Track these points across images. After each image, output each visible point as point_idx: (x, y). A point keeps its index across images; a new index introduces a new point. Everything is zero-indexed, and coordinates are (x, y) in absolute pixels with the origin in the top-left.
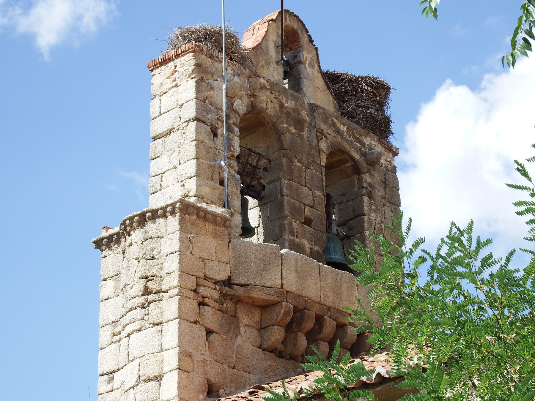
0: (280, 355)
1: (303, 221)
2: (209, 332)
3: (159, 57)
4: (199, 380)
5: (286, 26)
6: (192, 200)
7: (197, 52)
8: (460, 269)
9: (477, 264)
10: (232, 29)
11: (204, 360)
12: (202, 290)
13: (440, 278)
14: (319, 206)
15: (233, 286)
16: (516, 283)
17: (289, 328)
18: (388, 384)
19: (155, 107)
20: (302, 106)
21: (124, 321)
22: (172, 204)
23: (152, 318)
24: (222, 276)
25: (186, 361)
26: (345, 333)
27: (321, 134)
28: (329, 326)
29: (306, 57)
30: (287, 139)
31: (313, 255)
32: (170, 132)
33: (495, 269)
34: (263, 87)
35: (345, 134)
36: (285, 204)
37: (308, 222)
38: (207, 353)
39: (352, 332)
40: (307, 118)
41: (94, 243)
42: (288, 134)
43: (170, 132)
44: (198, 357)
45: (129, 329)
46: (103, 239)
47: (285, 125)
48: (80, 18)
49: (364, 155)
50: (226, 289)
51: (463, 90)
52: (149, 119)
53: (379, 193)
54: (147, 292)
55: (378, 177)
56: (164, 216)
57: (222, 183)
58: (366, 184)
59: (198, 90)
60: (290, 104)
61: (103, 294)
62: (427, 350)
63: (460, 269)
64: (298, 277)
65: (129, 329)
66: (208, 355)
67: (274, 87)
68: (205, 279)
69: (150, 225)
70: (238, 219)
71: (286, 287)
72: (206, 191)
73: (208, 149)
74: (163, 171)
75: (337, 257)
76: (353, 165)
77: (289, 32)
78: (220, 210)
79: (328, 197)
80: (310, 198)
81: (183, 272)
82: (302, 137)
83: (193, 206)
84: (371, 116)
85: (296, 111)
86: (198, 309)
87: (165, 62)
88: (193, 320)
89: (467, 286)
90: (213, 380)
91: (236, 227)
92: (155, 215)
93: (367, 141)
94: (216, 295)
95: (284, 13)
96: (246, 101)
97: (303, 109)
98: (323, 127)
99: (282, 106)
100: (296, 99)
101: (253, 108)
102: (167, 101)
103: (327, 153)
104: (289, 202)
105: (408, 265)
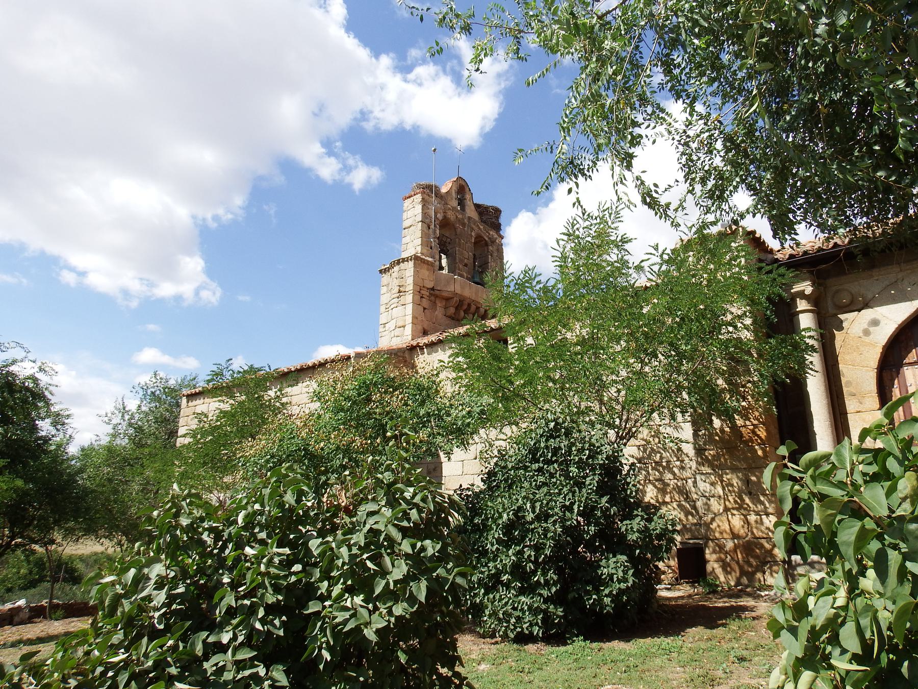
0: (453, 319)
2: (425, 309)
3: (407, 195)
4: (420, 327)
6: (419, 255)
7: (423, 193)
8: (527, 285)
9: (534, 283)
10: (437, 184)
12: (422, 292)
13: (519, 288)
16: (550, 291)
17: (457, 308)
19: (405, 216)
21: (390, 303)
23: (401, 303)
24: (430, 285)
25: (416, 321)
26: (479, 311)
27: (472, 229)
28: (473, 308)
30: (458, 231)
31: (468, 279)
33: (541, 286)
34: (450, 209)
37: (466, 265)
39: (482, 311)
44: (420, 318)
45: (392, 307)
48: (370, 177)
49: (489, 238)
50: (432, 292)
51: (530, 214)
52: (402, 221)
53: (495, 254)
54: (400, 292)
55: (495, 248)
56: (407, 261)
57: (431, 248)
59: (422, 209)
60: (460, 216)
61: (382, 292)
62: (511, 317)
63: (527, 285)
65: (392, 307)
67: (454, 209)
69: (402, 264)
70: (437, 263)
71: (456, 291)
72: (425, 251)
73: (426, 234)
75: (477, 280)
78: (430, 259)
79: (474, 255)
81: (415, 284)
83: (419, 257)
84: (493, 222)
85: (463, 219)
86: (685, 193)
87: (409, 197)
89: (529, 291)
90: (426, 328)
92: (404, 260)
93: (491, 233)
94: (428, 294)
95: (460, 178)
96: (442, 214)
98: (474, 226)
99: (457, 217)
100: (463, 214)
101: (445, 217)
102: (410, 213)
105: (506, 281)
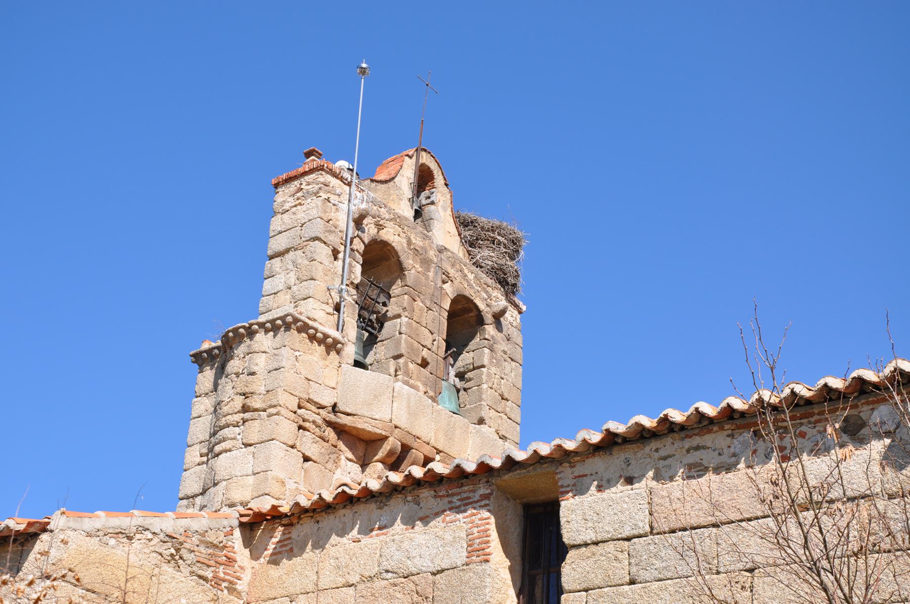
1: (419, 362)
5: (423, 165)
11: (297, 489)
14: (379, 566)
15: (338, 414)
18: (518, 471)
19: (276, 223)
20: (430, 246)
22: (282, 317)
29: (439, 199)
32: (287, 251)
35: (472, 282)
36: (403, 342)
38: (302, 483)
40: (435, 258)
41: (191, 356)
42: (413, 271)
43: (287, 251)
46: (201, 352)
47: (411, 262)
52: (266, 237)
58: (489, 336)
64: (409, 414)
66: (302, 485)
68: (309, 402)
74: (276, 291)
76: (477, 315)
77: (424, 171)
80: (430, 340)
82: (427, 277)
88: (290, 443)
91: (349, 357)
97: (431, 248)
98: (452, 272)
103: (452, 298)
104: (406, 341)
